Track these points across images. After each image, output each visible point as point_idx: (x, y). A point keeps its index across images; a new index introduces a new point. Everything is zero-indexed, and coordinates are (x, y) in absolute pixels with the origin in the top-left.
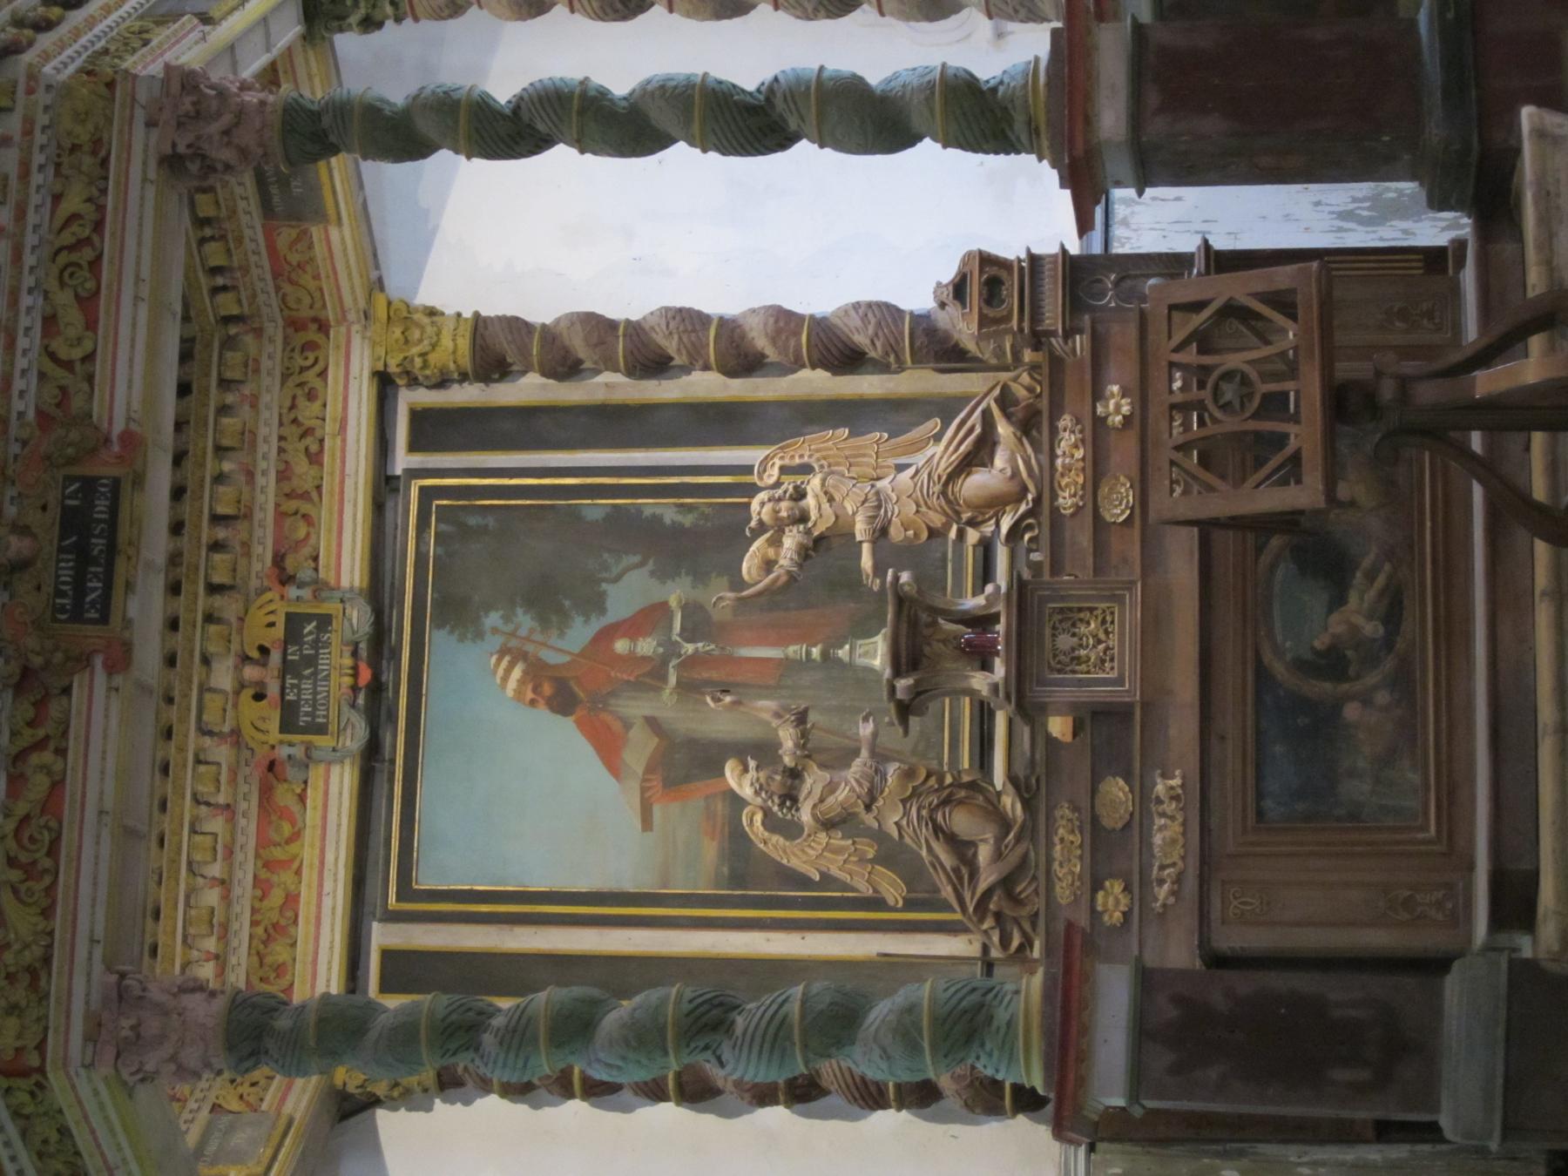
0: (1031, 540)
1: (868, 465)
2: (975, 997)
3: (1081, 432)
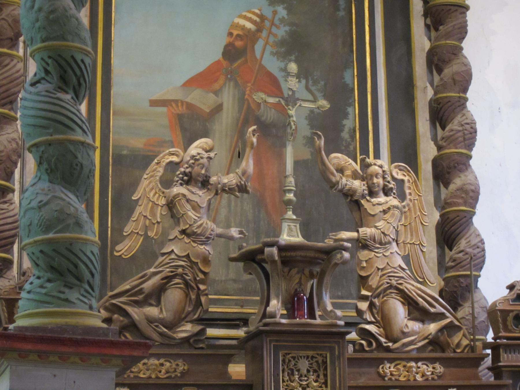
0: (362, 345)
1: (406, 237)
2: (87, 275)
3: (433, 379)
